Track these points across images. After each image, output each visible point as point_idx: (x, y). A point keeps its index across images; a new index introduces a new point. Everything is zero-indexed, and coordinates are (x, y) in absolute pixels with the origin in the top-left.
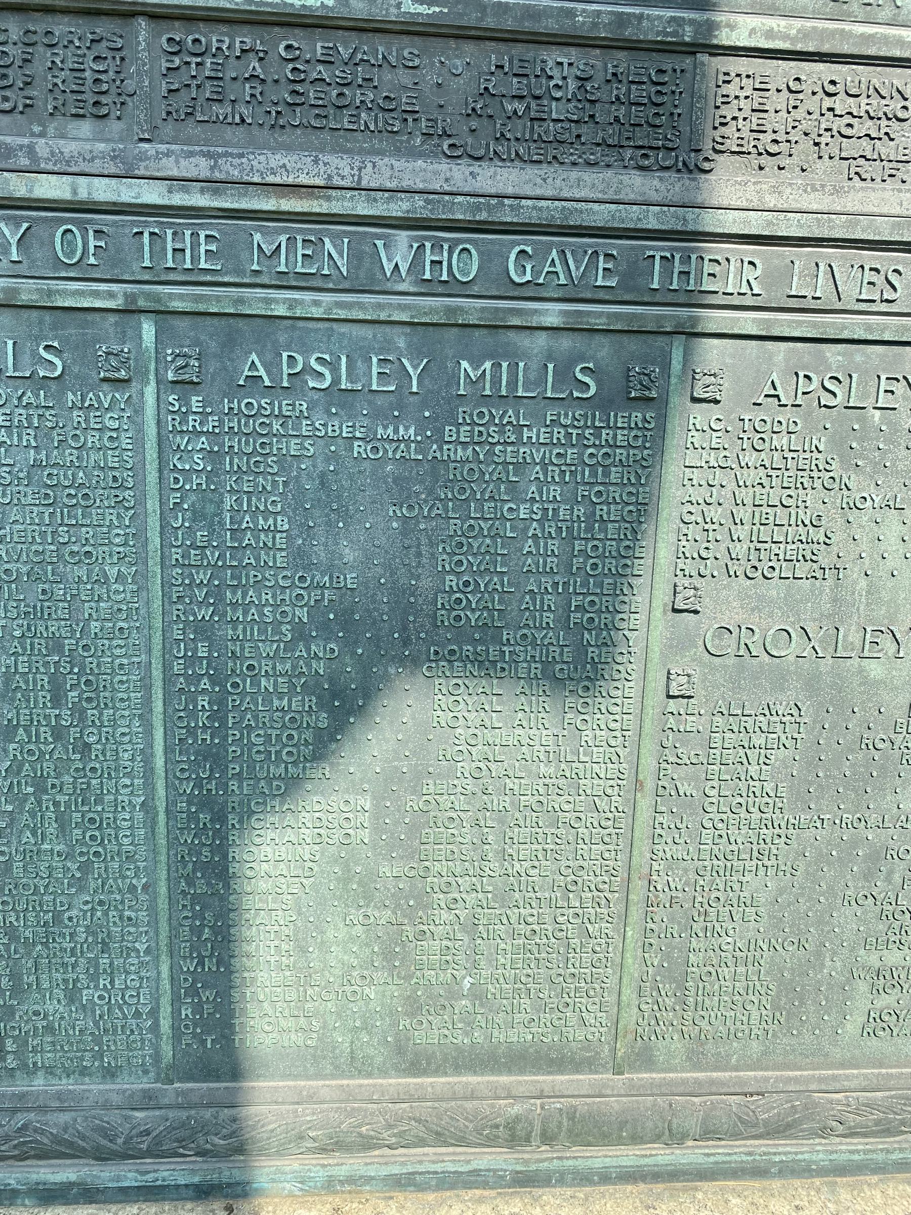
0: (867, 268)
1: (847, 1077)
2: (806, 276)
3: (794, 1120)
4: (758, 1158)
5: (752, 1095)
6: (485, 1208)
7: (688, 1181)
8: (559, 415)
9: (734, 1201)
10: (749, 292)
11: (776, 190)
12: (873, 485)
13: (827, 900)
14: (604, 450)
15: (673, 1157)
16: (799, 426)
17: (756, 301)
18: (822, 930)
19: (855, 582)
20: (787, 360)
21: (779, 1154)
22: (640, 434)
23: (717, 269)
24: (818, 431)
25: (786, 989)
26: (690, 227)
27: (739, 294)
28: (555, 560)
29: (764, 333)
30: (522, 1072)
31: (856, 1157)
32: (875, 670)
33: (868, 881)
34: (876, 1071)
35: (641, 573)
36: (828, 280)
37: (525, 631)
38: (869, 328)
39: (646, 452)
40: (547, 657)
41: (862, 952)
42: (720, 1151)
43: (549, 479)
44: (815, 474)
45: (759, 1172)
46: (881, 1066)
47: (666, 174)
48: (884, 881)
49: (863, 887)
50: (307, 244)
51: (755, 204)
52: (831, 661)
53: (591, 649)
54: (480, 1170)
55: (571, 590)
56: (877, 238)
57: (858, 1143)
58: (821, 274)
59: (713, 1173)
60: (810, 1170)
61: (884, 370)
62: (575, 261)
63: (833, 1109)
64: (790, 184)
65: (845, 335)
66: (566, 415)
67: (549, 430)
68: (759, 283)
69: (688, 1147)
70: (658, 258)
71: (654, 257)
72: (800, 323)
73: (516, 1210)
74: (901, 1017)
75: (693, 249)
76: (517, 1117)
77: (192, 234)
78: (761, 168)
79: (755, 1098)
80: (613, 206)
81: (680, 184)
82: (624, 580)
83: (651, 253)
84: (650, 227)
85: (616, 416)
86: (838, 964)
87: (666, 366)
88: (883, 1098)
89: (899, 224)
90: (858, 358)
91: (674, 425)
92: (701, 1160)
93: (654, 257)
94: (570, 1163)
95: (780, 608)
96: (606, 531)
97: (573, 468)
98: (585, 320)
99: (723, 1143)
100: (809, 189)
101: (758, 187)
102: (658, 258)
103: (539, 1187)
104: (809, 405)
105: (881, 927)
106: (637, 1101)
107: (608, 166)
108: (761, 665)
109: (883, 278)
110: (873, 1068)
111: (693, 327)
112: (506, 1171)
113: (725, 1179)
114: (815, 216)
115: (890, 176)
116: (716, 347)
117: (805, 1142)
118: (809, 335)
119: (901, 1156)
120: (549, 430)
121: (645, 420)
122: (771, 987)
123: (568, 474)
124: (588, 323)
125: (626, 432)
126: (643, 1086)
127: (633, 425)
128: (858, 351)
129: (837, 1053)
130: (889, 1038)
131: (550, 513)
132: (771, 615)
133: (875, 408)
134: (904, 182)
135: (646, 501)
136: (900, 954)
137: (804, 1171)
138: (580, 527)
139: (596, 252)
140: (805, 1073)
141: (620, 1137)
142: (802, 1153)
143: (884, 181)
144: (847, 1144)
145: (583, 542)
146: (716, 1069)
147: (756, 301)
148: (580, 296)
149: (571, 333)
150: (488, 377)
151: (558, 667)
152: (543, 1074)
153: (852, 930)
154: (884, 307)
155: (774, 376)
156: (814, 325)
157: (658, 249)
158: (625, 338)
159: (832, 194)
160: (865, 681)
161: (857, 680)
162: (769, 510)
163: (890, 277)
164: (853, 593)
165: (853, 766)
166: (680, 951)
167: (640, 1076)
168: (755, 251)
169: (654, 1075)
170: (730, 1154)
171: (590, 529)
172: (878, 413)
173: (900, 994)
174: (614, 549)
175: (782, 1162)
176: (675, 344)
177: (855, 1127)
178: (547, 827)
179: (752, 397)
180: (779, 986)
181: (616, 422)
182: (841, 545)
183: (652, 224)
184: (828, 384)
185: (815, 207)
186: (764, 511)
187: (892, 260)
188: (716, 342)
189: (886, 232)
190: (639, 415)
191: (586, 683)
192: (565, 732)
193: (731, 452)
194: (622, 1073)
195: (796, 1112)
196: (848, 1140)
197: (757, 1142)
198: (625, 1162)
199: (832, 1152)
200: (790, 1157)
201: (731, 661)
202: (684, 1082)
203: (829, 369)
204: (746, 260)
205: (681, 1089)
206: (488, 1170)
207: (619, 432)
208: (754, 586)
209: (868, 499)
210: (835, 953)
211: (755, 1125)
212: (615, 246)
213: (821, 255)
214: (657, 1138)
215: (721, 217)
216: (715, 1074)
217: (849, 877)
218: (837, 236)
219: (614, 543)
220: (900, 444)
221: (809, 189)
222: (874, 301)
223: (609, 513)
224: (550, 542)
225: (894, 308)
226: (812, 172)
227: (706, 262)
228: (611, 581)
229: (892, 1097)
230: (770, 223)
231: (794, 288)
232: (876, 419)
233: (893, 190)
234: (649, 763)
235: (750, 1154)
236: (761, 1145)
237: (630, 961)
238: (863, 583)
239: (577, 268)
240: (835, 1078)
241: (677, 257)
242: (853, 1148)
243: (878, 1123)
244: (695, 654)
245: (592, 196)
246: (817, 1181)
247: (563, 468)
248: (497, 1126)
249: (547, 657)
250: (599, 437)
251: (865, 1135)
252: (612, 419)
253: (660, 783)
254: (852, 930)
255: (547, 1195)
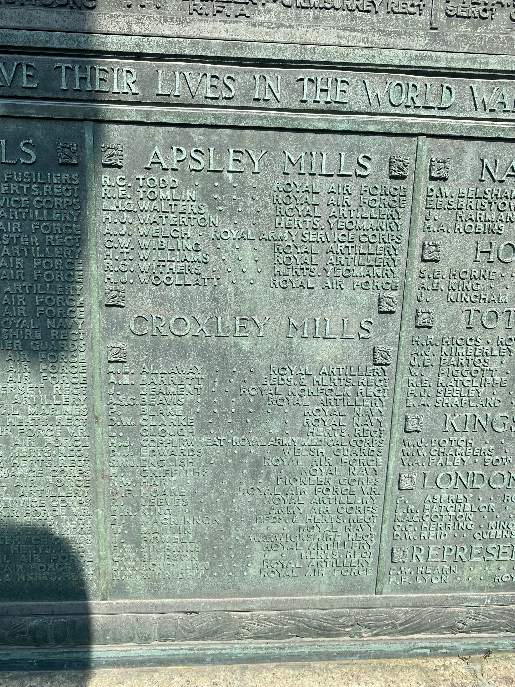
0: (209, 75)
1: (252, 602)
2: (168, 81)
3: (218, 629)
4: (196, 652)
5: (191, 614)
6: (16, 683)
7: (153, 666)
8: (12, 174)
9: (176, 679)
10: (130, 91)
11: (138, 21)
12: (232, 224)
13: (229, 491)
14: (47, 198)
15: (141, 651)
16: (177, 183)
17: (136, 98)
18: (228, 511)
19: (226, 288)
20: (165, 139)
21: (210, 649)
22: (69, 188)
23: (106, 76)
24: (191, 187)
25: (208, 547)
26: (83, 47)
27: (124, 93)
28: (22, 271)
29: (145, 120)
30: (41, 599)
31: (260, 652)
32: (245, 344)
33: (254, 479)
34: (271, 598)
35: (81, 280)
36: (183, 84)
37: (7, 319)
38: (216, 116)
39: (75, 200)
40: (24, 336)
41: (255, 524)
42: (172, 648)
43: (12, 218)
44: (192, 216)
45: (198, 661)
46: (275, 595)
47: (62, 10)
48: (265, 479)
49: (252, 483)
50: (29, 68)
51: (126, 30)
52: (215, 339)
53: (53, 331)
54: (17, 659)
55: (35, 292)
56: (213, 55)
57: (263, 643)
58: (177, 79)
59: (169, 661)
60: (232, 660)
61: (233, 146)
62: (7, 70)
63: (243, 622)
64: (149, 17)
65: (201, 121)
66: (18, 175)
67: (7, 184)
68: (137, 86)
69: (152, 645)
70: (63, 68)
71: (60, 67)
72: (168, 113)
73: (35, 684)
74: (285, 565)
75: (88, 63)
76: (35, 627)
77: (91, 68)
78: (129, 6)
79: (193, 615)
80: (28, 32)
81: (72, 17)
82: (70, 285)
83: (58, 65)
84: (55, 46)
85: (51, 176)
86: (240, 532)
87: (82, 143)
88: (275, 615)
89: (227, 45)
90: (214, 138)
91: (91, 180)
92: (160, 653)
93: (60, 67)
94: (75, 655)
95: (178, 304)
96: (54, 252)
97: (27, 210)
98: (21, 110)
99: (175, 643)
100: (162, 21)
101: (127, 19)
102: (63, 68)
103: (56, 670)
104: (183, 169)
105: (266, 508)
106: (115, 617)
107: (22, 4)
108: (170, 341)
109: (222, 83)
110: (270, 596)
111: (96, 116)
112: (33, 660)
113: (176, 665)
114: (169, 39)
115: (218, 11)
116: (116, 130)
117: (228, 642)
118: (177, 122)
119: (290, 651)
120: (7, 184)
121: (71, 178)
122: (197, 546)
123: (24, 214)
124: (23, 113)
125: (60, 186)
126: (119, 608)
127: (64, 182)
128: (213, 133)
129: (245, 587)
130: (278, 578)
131: (15, 240)
132: (172, 309)
133: (228, 171)
134: (228, 16)
135: (79, 232)
136: (280, 526)
137: (227, 660)
138: (35, 249)
139: (20, 64)
140: (225, 599)
141: (106, 639)
142: (225, 649)
143: (215, 15)
144: (255, 643)
145: (40, 260)
146: (167, 597)
147: (136, 98)
148: (14, 94)
149: (15, 119)
150: (303, 160)
151: (32, 343)
152: (55, 601)
153: (247, 510)
154: (225, 103)
155: (156, 149)
156: (179, 115)
157: (64, 62)
158: (53, 124)
159: (179, 24)
160: (239, 351)
161: (233, 351)
162: (163, 240)
163: (226, 82)
164: (226, 295)
165: (237, 405)
166: (135, 524)
167: (118, 601)
168: (131, 64)
169: (127, 601)
170: (178, 650)
171: (42, 251)
172: (231, 175)
173: (282, 551)
174: (60, 264)
175: (212, 654)
176: (87, 128)
177: (258, 633)
178: (38, 446)
179: (144, 163)
180: (203, 545)
181: (52, 180)
182: (214, 263)
183: (57, 44)
184: (361, 162)
185: (167, 33)
186: (159, 240)
187: (228, 70)
188: (115, 126)
189: (219, 50)
190: (67, 175)
191: (52, 353)
192: (43, 385)
193: (133, 200)
194: (106, 600)
195: (218, 625)
196: (256, 641)
197: (197, 642)
198: (110, 654)
199: (244, 649)
200: (218, 652)
201: (149, 339)
202: (146, 605)
203: (194, 145)
204: (125, 69)
205: (143, 610)
206: (22, 659)
207: (55, 186)
208: (159, 290)
209: (229, 233)
210: (237, 525)
211: (193, 632)
212: (33, 60)
213: (256, 71)
214: (131, 640)
215: (103, 40)
216: (166, 601)
217: (241, 477)
218: (186, 53)
219: (60, 260)
220: (247, 196)
221: (162, 21)
222: (217, 98)
223: (54, 240)
224: (17, 260)
225: (232, 103)
226: (164, 9)
227: (97, 71)
228: (61, 286)
229: (281, 615)
230: (137, 44)
231: (160, 89)
232: (230, 179)
233: (220, 21)
234: (100, 404)
235: (191, 649)
236: (199, 644)
237: (103, 530)
238: (231, 288)
239: (9, 75)
240: (243, 602)
241: (77, 67)
242: (259, 646)
243: (272, 630)
244: (124, 334)
245: (12, 25)
246: (235, 666)
247: (20, 210)
248: (23, 633)
249: (24, 336)
250: (42, 189)
251: (266, 638)
252: (49, 178)
253: (110, 417)
254: (247, 510)
255: (59, 676)
